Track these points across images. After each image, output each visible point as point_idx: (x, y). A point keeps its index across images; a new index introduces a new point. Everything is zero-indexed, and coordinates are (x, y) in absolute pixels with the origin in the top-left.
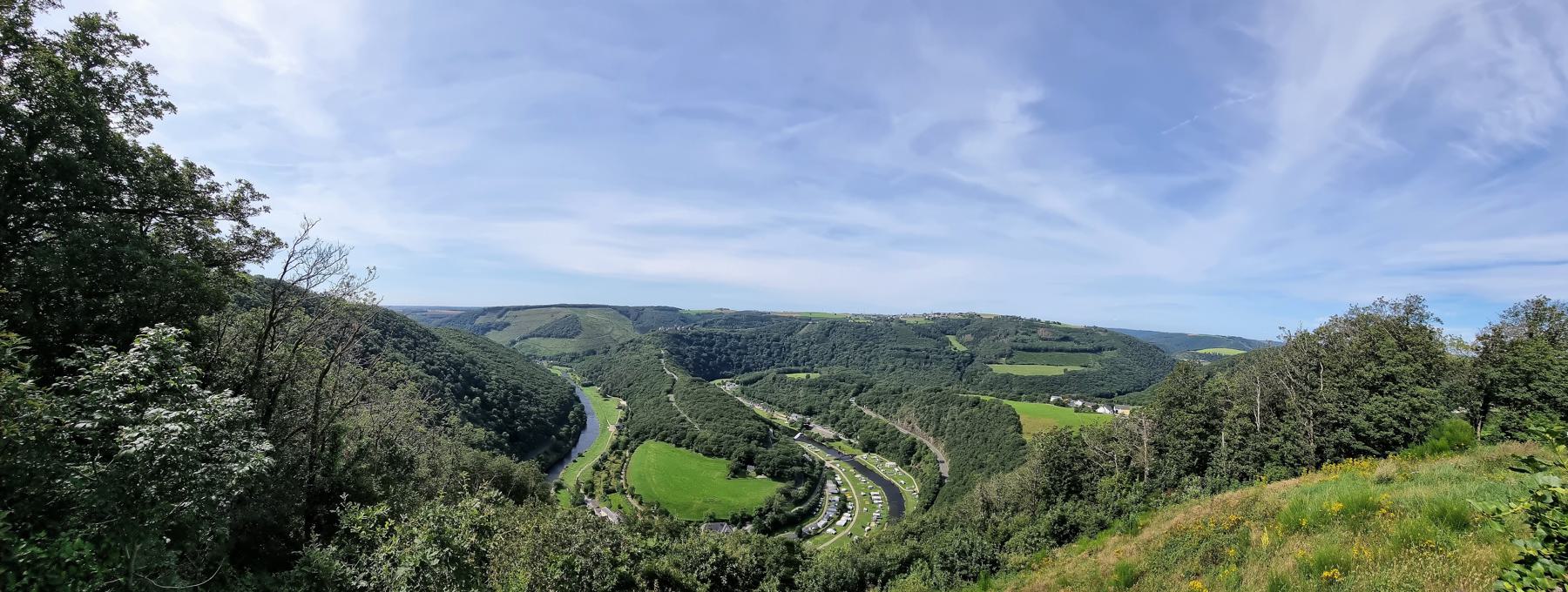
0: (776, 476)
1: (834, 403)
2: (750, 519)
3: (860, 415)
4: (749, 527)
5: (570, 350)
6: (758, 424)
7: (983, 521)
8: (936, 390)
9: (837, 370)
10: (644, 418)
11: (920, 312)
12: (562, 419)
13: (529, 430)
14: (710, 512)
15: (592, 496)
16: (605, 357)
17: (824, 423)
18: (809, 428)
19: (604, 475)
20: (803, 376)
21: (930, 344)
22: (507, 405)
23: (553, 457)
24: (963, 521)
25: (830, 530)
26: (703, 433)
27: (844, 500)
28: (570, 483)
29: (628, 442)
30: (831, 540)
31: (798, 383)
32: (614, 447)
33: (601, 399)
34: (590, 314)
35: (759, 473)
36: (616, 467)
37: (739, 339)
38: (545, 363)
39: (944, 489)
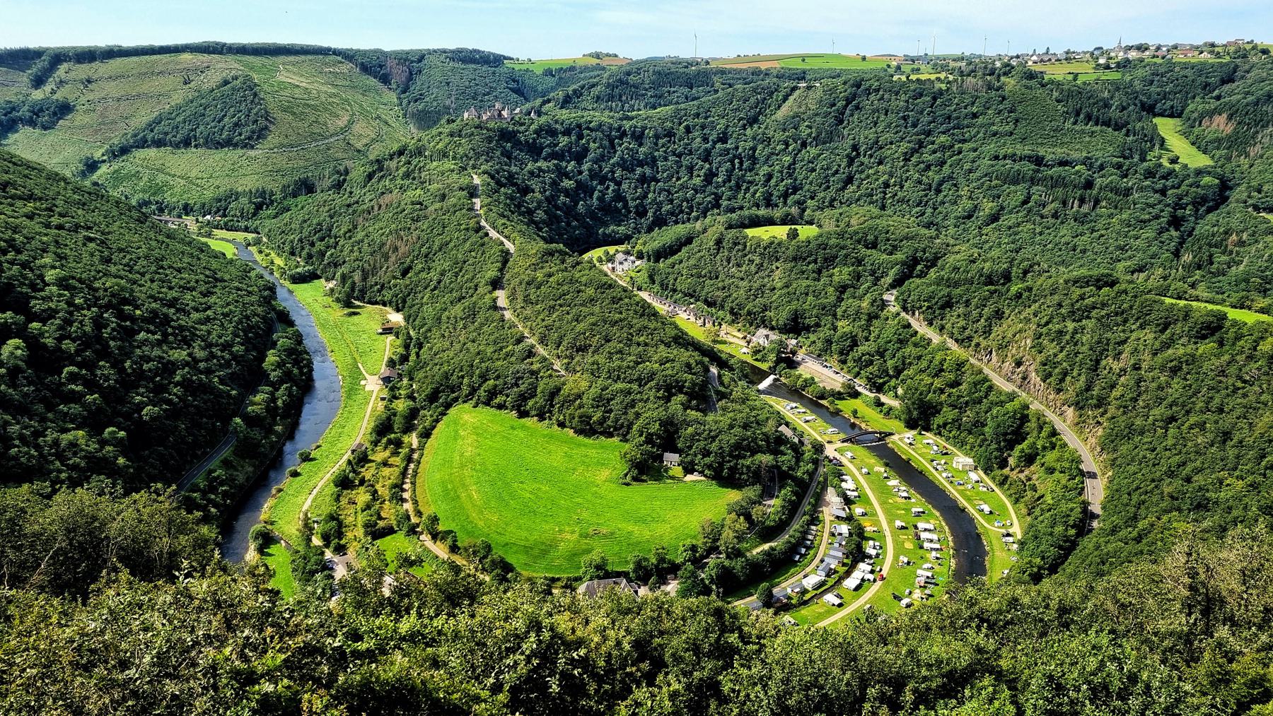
0: (726, 477)
1: (849, 303)
2: (674, 569)
3: (905, 336)
4: (672, 587)
5: (249, 182)
6: (686, 355)
7: (1188, 639)
8: (1103, 282)
9: (859, 216)
10: (447, 352)
11: (1084, 45)
12: (252, 377)
13: (175, 413)
14: (595, 556)
15: (341, 550)
16: (339, 200)
17: (821, 355)
18: (792, 364)
19: (362, 496)
20: (781, 232)
21: (1102, 145)
22: (104, 353)
23: (245, 471)
24: (1126, 620)
25: (830, 598)
26: (576, 382)
27: (859, 534)
28: (289, 528)
29: (413, 414)
30: (823, 614)
31: (771, 251)
32: (383, 429)
33: (338, 313)
34: (287, 75)
35: (689, 469)
36: (390, 474)
37: (639, 137)
38: (190, 222)
39: (1088, 543)
